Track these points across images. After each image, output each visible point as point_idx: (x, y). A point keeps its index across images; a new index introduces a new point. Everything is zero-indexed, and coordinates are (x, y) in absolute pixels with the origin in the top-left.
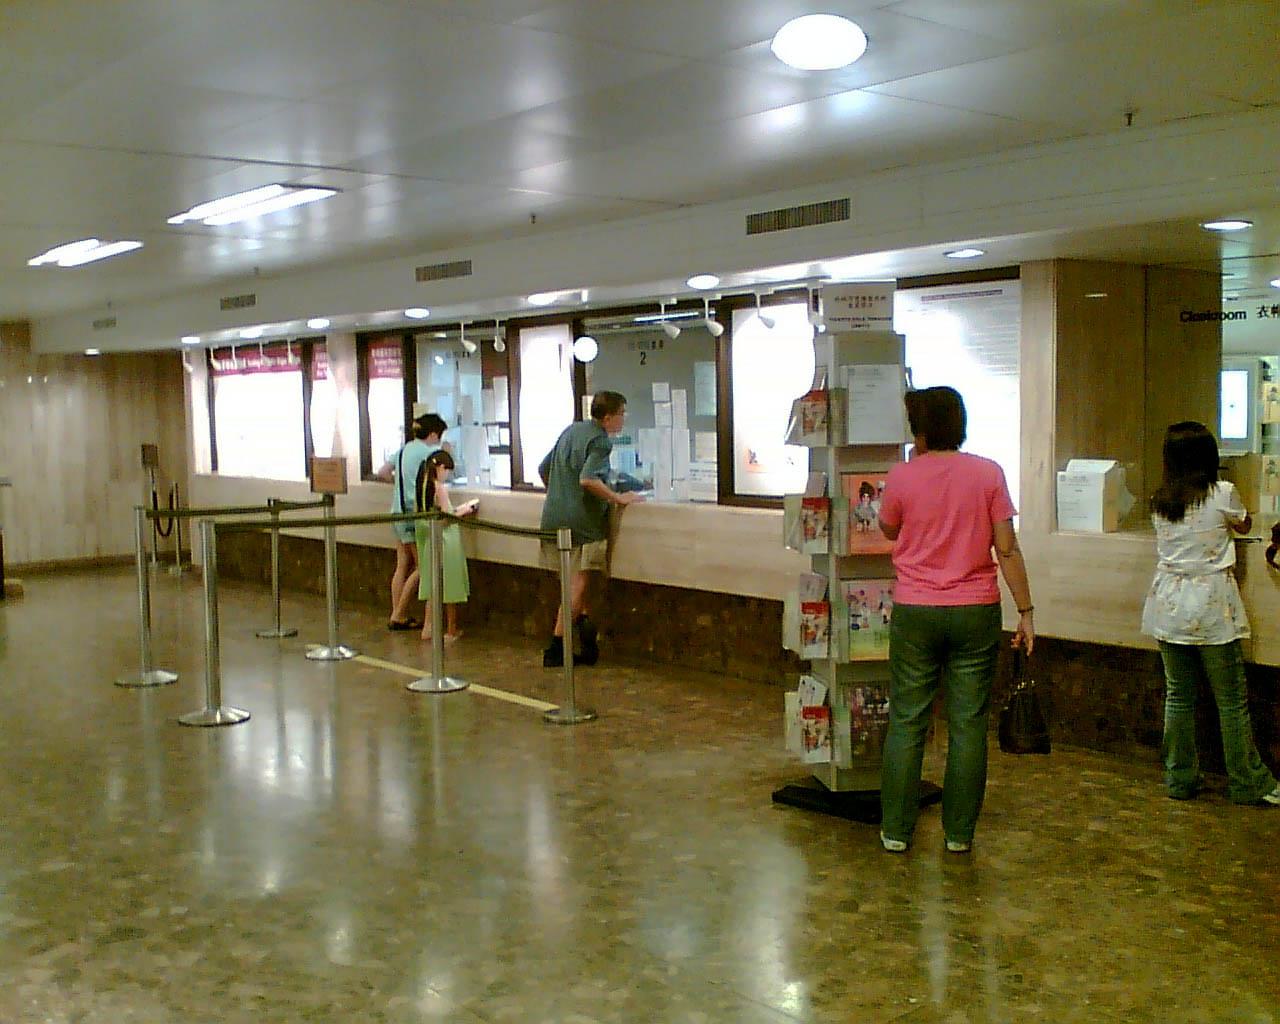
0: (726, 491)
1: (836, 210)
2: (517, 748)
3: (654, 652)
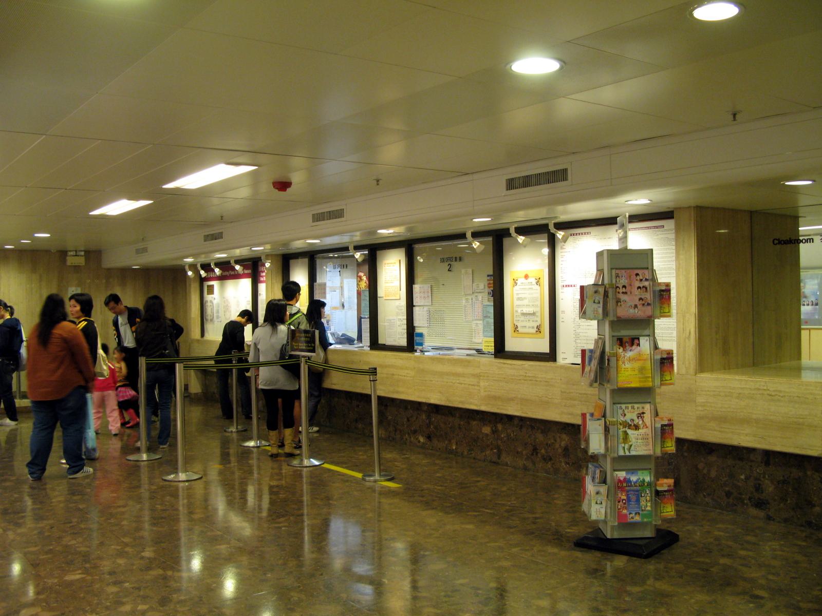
0: (500, 350)
1: (560, 175)
2: (363, 509)
3: (456, 448)
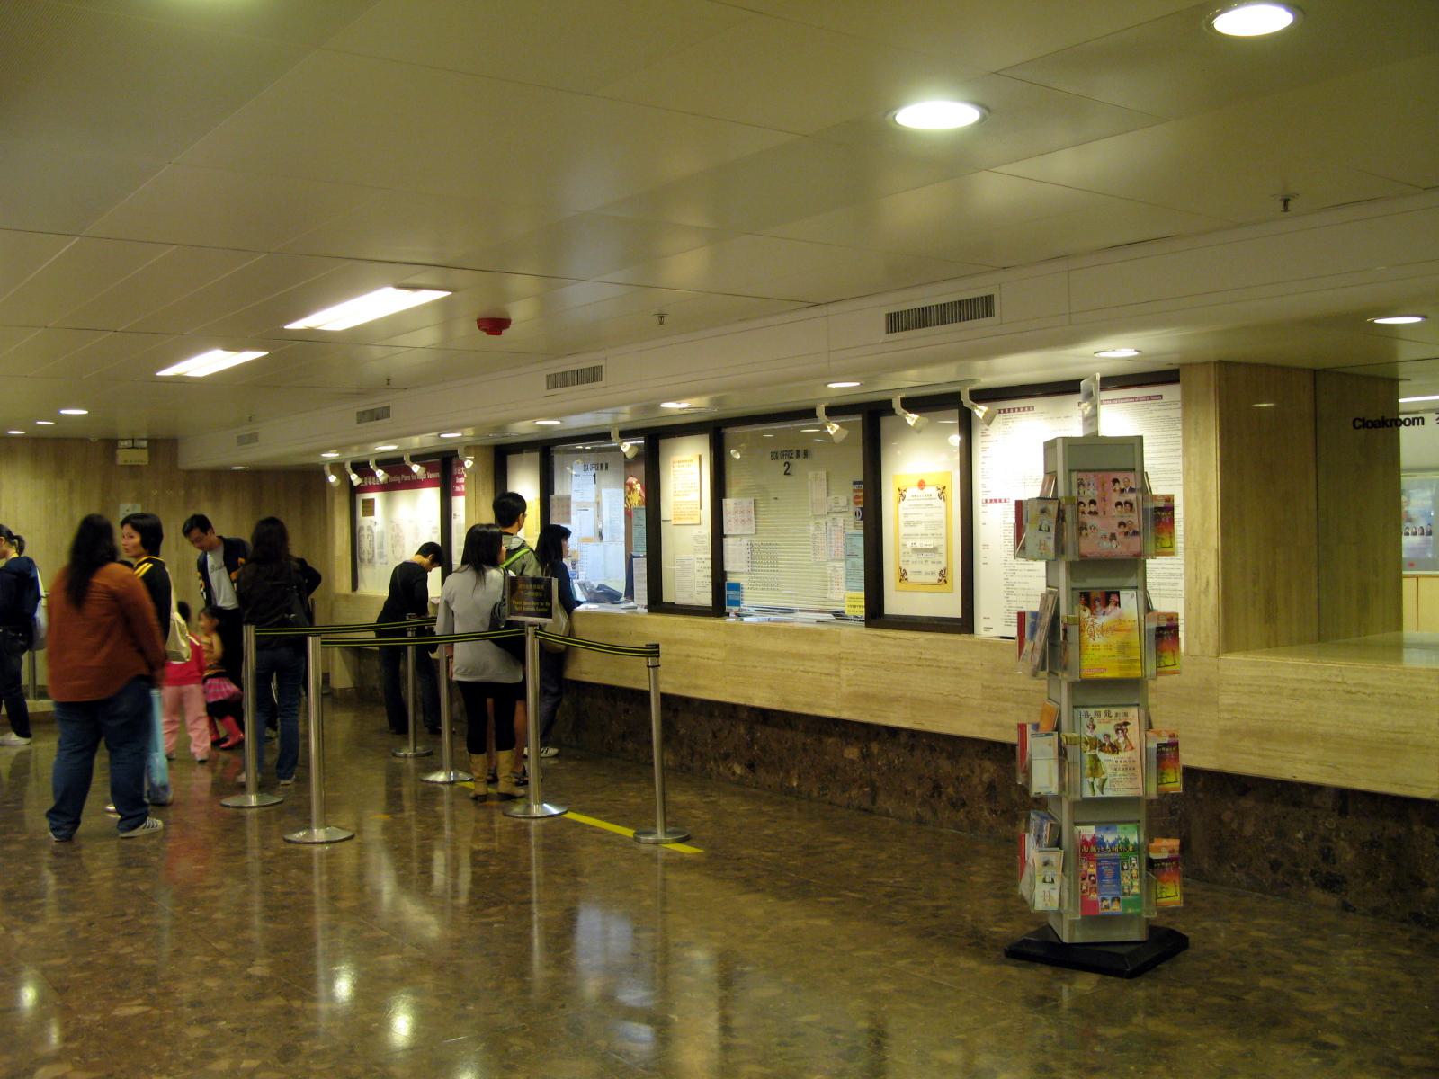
0: (875, 614)
1: (979, 307)
2: (636, 891)
3: (797, 786)
